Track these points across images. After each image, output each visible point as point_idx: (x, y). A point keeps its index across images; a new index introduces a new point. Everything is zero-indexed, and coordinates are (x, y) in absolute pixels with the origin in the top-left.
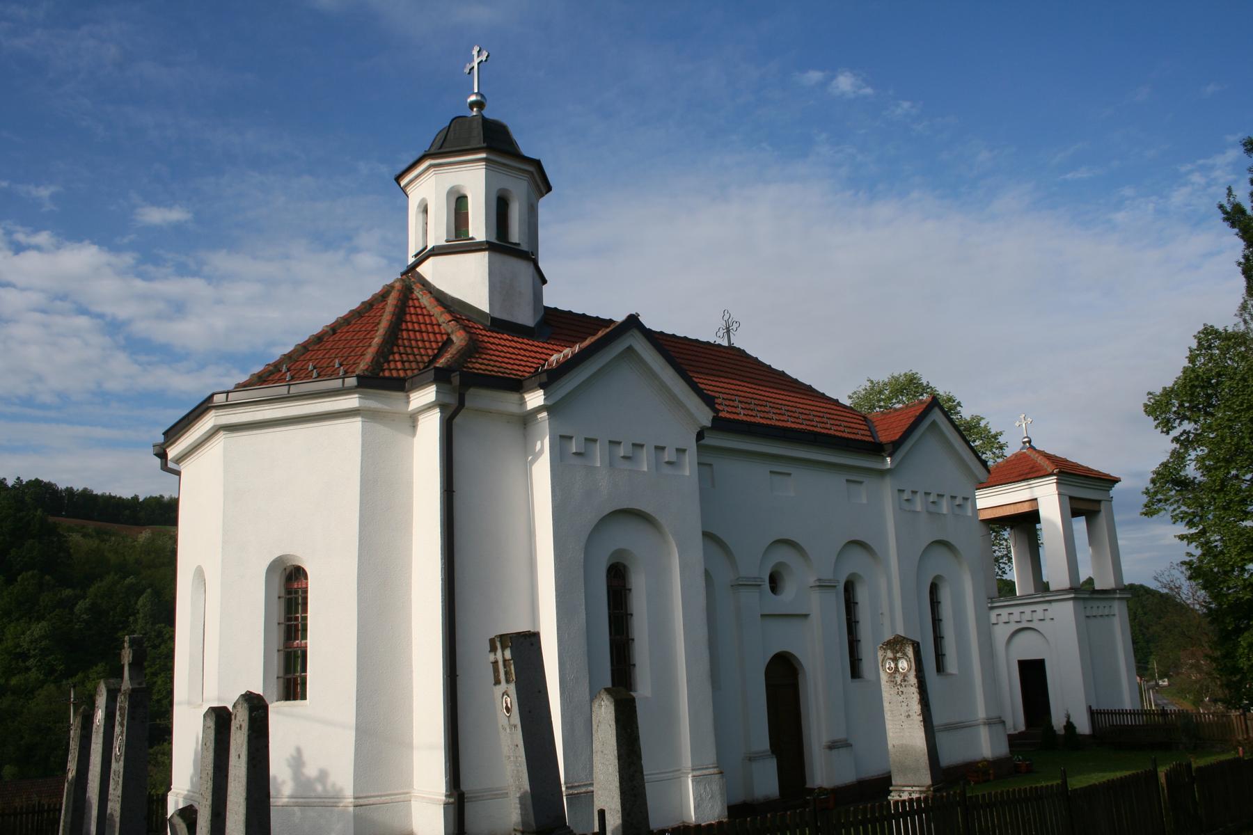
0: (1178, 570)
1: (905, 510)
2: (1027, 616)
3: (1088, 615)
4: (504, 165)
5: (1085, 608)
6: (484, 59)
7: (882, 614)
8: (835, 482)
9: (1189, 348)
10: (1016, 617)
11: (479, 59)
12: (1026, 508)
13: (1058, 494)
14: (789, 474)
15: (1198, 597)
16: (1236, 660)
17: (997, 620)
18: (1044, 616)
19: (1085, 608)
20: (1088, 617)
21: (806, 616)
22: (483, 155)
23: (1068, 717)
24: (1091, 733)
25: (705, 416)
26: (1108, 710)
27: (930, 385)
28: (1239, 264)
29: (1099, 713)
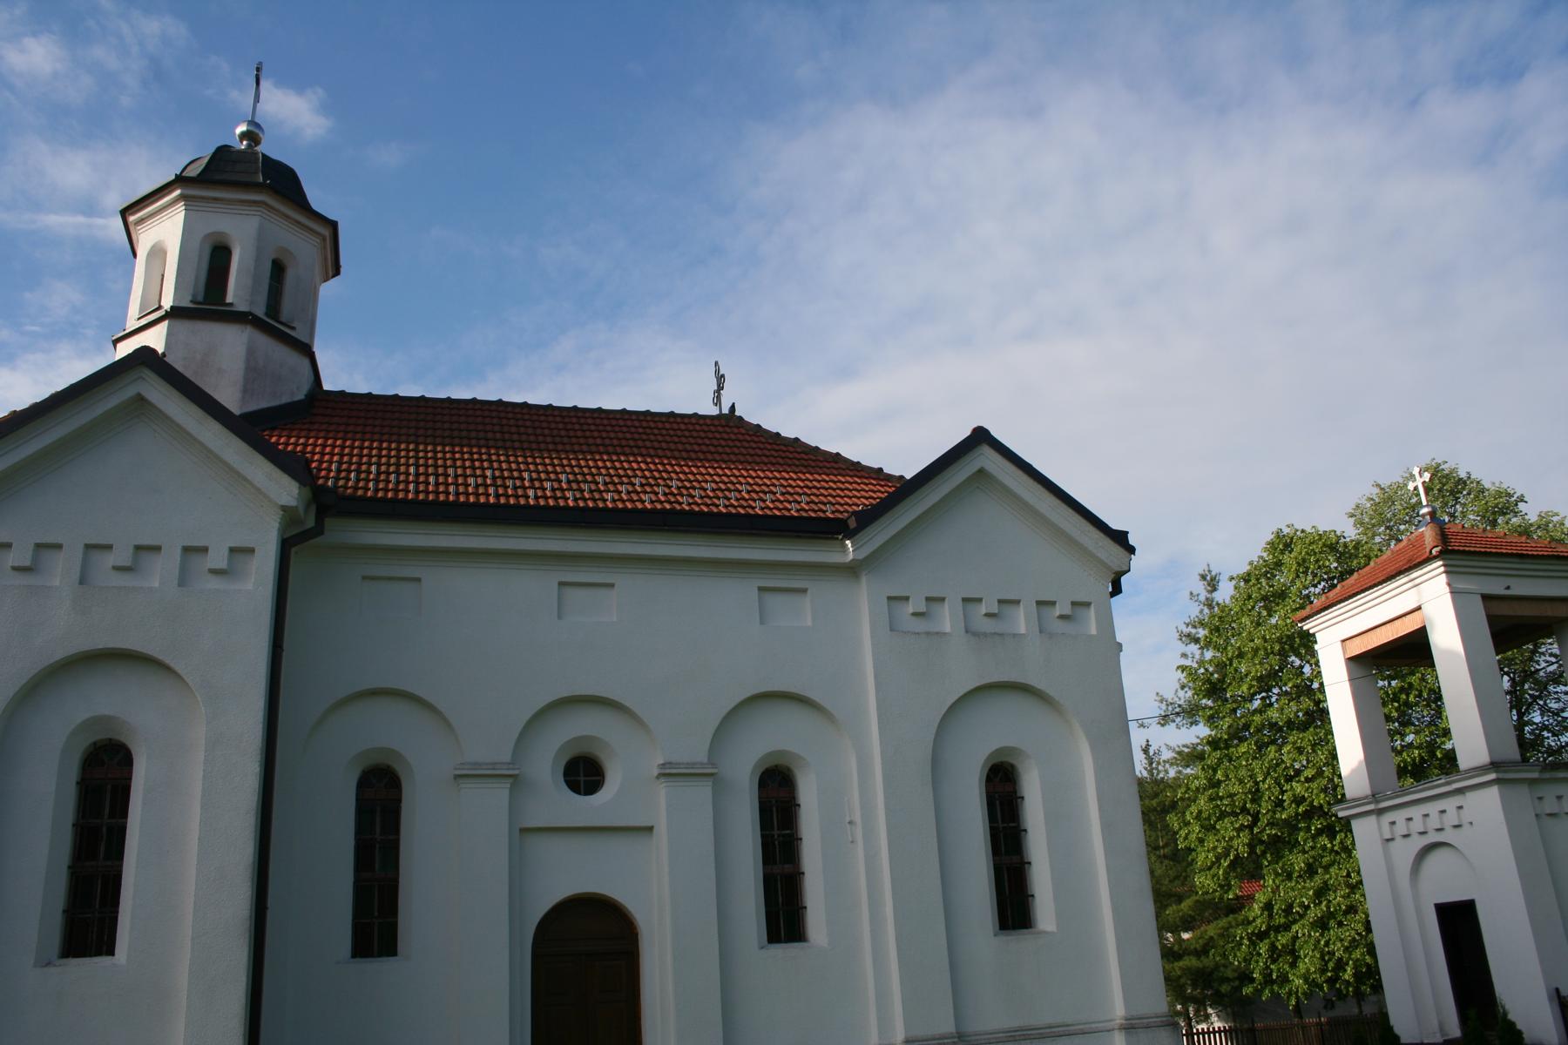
1: (985, 635)
2: (1434, 822)
4: (216, 199)
7: (850, 823)
8: (737, 594)
10: (1417, 825)
13: (1451, 592)
14: (612, 586)
17: (1392, 832)
18: (1442, 823)
21: (650, 829)
22: (178, 192)
25: (286, 491)
27: (1472, 477)
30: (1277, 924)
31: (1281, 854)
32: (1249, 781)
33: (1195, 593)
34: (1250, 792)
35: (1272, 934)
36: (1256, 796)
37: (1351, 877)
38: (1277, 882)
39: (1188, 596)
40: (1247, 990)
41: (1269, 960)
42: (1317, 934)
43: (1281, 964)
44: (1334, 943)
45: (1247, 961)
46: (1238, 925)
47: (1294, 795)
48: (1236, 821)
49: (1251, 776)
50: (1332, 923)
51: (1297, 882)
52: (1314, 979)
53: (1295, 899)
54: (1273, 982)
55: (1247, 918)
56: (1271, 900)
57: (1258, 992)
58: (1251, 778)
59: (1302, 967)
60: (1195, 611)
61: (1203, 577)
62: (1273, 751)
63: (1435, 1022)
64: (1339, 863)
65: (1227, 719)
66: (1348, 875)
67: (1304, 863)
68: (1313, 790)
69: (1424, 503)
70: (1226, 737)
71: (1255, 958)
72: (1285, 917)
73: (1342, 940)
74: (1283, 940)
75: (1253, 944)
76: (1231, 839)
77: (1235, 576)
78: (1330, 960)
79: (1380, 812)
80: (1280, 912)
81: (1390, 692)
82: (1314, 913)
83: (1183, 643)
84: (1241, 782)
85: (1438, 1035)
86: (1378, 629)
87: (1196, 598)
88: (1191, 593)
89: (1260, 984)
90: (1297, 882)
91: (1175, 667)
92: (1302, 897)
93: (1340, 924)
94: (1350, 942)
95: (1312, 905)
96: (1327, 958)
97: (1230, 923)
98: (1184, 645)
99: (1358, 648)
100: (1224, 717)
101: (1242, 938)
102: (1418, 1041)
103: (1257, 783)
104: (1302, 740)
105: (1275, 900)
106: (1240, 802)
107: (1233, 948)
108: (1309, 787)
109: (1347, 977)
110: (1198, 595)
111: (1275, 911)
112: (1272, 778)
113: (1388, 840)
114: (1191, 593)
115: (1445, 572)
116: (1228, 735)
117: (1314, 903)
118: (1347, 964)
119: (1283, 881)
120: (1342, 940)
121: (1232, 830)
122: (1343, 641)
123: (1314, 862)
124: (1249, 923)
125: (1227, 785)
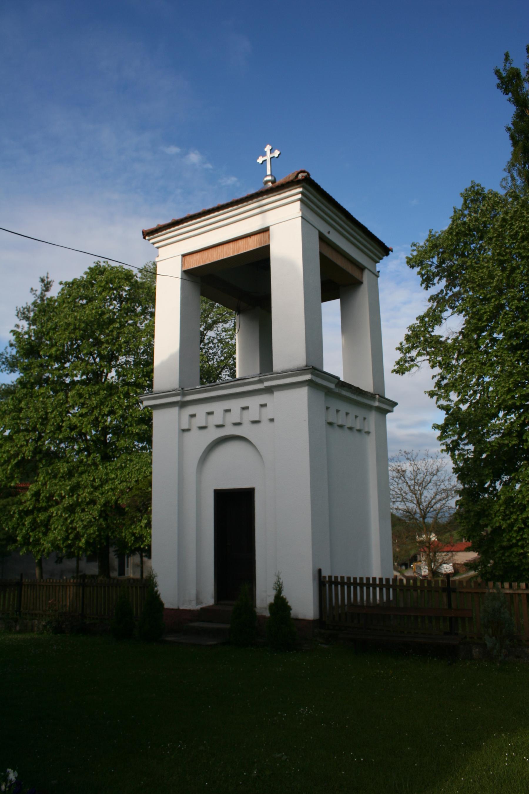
0: (405, 456)
2: (234, 417)
3: (330, 420)
5: (327, 408)
6: (276, 155)
9: (454, 208)
10: (217, 419)
11: (272, 156)
12: (252, 244)
15: (418, 480)
16: (490, 518)
17: (190, 423)
19: (327, 408)
20: (330, 424)
23: (279, 589)
24: (317, 617)
26: (349, 578)
28: (509, 129)
29: (334, 582)
30: (40, 506)
31: (52, 461)
32: (42, 411)
33: (34, 289)
34: (41, 418)
35: (36, 512)
36: (45, 420)
37: (95, 482)
38: (46, 479)
39: (29, 290)
40: (11, 548)
41: (30, 530)
42: (67, 515)
43: (37, 533)
44: (77, 522)
45: (15, 529)
46: (13, 504)
47: (70, 424)
48: (28, 435)
49: (43, 408)
50: (78, 509)
51: (60, 481)
52: (58, 544)
53: (57, 491)
54: (29, 544)
55: (20, 500)
56: (39, 490)
57: (17, 550)
58: (44, 409)
59: (51, 536)
60: (30, 299)
61: (42, 280)
62: (62, 395)
63: (193, 592)
64: (89, 473)
65: (36, 369)
66: (94, 480)
67: (67, 468)
68: (84, 421)
69: (269, 173)
70: (33, 381)
71: (21, 527)
72: (47, 502)
73: (82, 521)
74: (42, 517)
75: (21, 518)
76: (22, 446)
77: (63, 282)
78: (71, 533)
79: (183, 405)
80: (44, 498)
81: (145, 371)
82: (67, 502)
83: (18, 318)
84: (37, 410)
85: (194, 603)
86: (220, 248)
87: (34, 292)
88: (32, 289)
89: (21, 544)
90: (60, 481)
91: (10, 330)
92: (61, 490)
93: (83, 510)
94: (88, 522)
95: (67, 496)
96: (70, 531)
97: (8, 502)
98: (18, 320)
99: (195, 262)
100: (35, 368)
101: (14, 513)
102: (175, 607)
103: (47, 413)
104: (84, 389)
105: (43, 490)
106: (33, 424)
107: (6, 519)
108: (81, 420)
109: (81, 544)
110: (36, 290)
111: (41, 497)
112: (58, 411)
113: (184, 431)
114: (32, 289)
115: (301, 200)
116: (35, 380)
117: (69, 495)
118: (83, 536)
119: (50, 478)
120: (82, 521)
121: (24, 441)
122: (184, 256)
123: (73, 470)
124: (21, 503)
125: (27, 411)
